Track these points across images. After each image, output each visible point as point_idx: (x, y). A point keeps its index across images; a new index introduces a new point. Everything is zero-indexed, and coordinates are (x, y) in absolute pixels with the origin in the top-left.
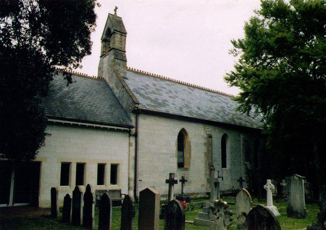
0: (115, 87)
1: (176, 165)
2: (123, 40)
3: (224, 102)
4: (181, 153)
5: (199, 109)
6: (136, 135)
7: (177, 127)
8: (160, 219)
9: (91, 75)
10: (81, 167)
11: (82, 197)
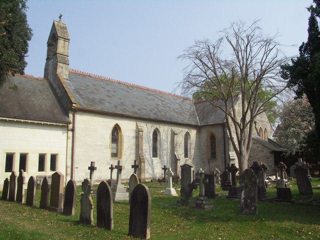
0: (57, 88)
1: (109, 155)
2: (66, 45)
3: (160, 100)
4: (115, 145)
5: (133, 106)
6: (73, 130)
7: (111, 122)
8: (6, 172)
9: (36, 76)
10: (24, 158)
11: (16, 179)
